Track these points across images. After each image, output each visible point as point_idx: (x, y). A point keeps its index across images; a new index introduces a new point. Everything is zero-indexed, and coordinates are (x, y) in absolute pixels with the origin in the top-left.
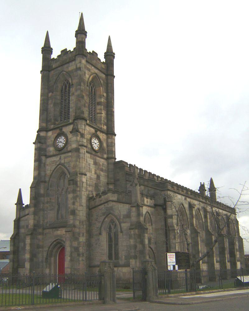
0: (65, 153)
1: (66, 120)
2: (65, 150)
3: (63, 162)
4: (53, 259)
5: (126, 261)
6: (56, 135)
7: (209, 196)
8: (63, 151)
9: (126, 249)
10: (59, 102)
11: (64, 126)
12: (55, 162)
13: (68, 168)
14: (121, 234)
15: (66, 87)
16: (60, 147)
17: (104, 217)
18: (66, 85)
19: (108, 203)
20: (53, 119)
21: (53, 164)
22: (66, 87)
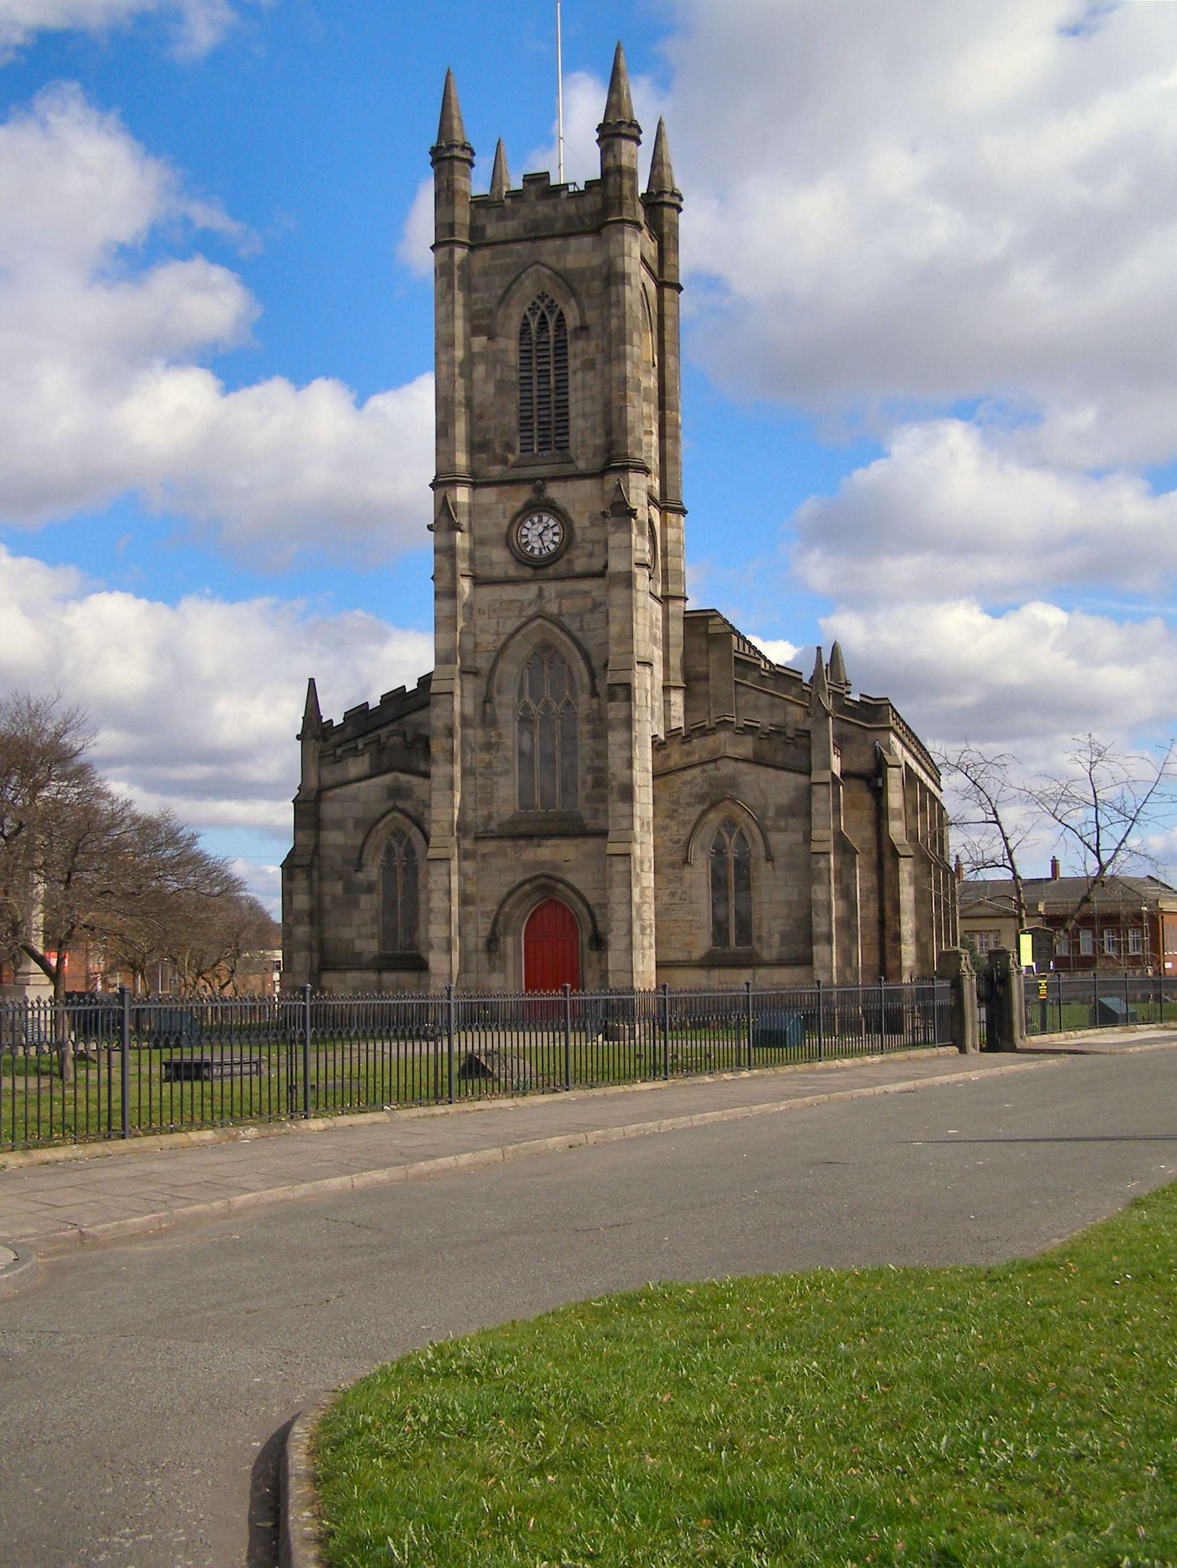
1: (545, 453)
2: (561, 567)
3: (552, 608)
4: (510, 940)
5: (784, 949)
6: (518, 505)
8: (550, 571)
9: (785, 911)
10: (514, 376)
11: (554, 479)
12: (518, 604)
13: (578, 634)
14: (769, 865)
15: (543, 323)
16: (536, 552)
17: (705, 807)
18: (543, 316)
19: (718, 763)
20: (497, 442)
21: (510, 614)
22: (543, 323)
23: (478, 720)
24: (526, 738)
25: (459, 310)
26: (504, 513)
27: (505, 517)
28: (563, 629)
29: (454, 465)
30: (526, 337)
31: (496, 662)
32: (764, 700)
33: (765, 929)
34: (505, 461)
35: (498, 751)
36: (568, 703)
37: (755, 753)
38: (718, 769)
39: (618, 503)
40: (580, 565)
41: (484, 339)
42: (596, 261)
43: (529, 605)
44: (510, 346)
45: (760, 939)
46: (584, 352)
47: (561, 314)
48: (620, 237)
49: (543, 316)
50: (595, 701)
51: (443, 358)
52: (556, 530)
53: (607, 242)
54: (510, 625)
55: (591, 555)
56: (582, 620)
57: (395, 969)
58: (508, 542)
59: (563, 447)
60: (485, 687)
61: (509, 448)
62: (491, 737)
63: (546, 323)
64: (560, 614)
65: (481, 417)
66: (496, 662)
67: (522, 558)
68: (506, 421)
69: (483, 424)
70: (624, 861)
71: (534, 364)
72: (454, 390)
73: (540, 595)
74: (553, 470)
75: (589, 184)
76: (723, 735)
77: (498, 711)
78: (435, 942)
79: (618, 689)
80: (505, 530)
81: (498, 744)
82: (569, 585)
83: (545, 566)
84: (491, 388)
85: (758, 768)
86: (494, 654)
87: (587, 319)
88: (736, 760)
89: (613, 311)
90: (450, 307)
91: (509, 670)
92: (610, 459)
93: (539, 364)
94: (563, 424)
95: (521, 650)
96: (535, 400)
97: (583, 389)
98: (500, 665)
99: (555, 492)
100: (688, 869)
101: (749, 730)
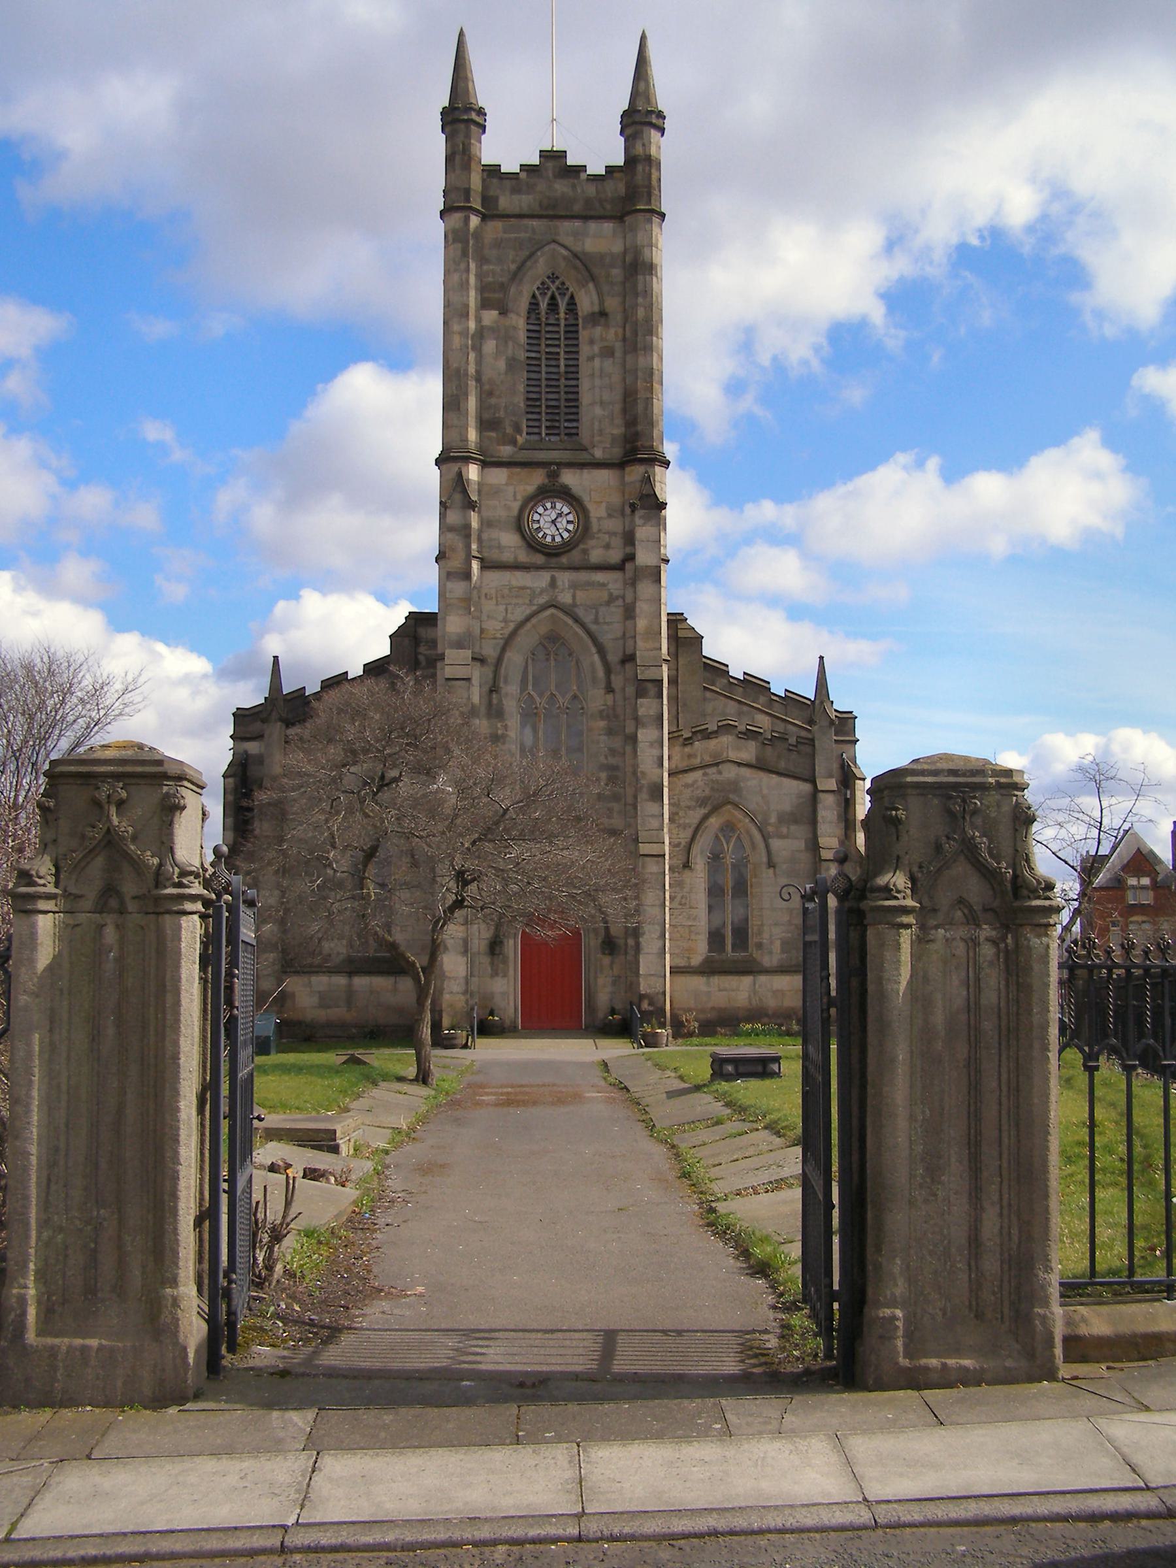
0: (576, 569)
1: (553, 438)
2: (575, 556)
3: (566, 598)
4: (511, 942)
6: (531, 489)
7: (862, 849)
8: (564, 560)
9: (786, 918)
10: (522, 355)
13: (593, 627)
14: (771, 871)
15: (553, 306)
17: (704, 811)
18: (553, 298)
21: (520, 601)
22: (553, 306)
23: (483, 710)
24: (528, 731)
25: (472, 280)
26: (515, 496)
27: (515, 500)
28: (577, 620)
29: (467, 440)
30: (533, 316)
31: (503, 650)
32: (732, 707)
33: (766, 935)
34: (514, 442)
35: (504, 743)
36: (575, 697)
37: (757, 759)
38: (720, 773)
39: (648, 496)
40: (596, 555)
41: (495, 313)
42: (617, 247)
43: (541, 592)
44: (519, 322)
45: (759, 946)
46: (602, 339)
47: (572, 297)
48: (648, 227)
49: (553, 298)
50: (610, 697)
51: (456, 327)
52: (570, 517)
53: (633, 229)
54: (519, 614)
55: (607, 546)
56: (597, 613)
57: (369, 973)
58: (519, 525)
59: (573, 434)
60: (491, 676)
61: (518, 430)
62: (497, 729)
63: (557, 305)
64: (574, 605)
65: (490, 394)
66: (503, 650)
67: (533, 544)
68: (516, 400)
69: (493, 401)
70: (658, 862)
71: (543, 346)
72: (467, 363)
73: (553, 583)
74: (565, 456)
75: (610, 169)
76: (726, 739)
77: (504, 702)
78: (450, 943)
79: (649, 685)
80: (515, 512)
81: (504, 736)
82: (583, 576)
83: (557, 555)
84: (502, 365)
85: (761, 774)
86: (502, 642)
87: (606, 304)
88: (739, 764)
89: (640, 300)
90: (464, 276)
91: (515, 658)
92: (635, 450)
93: (547, 346)
94: (574, 410)
95: (527, 640)
96: (544, 383)
97: (601, 377)
98: (508, 654)
99: (569, 478)
100: (687, 872)
101: (749, 735)
